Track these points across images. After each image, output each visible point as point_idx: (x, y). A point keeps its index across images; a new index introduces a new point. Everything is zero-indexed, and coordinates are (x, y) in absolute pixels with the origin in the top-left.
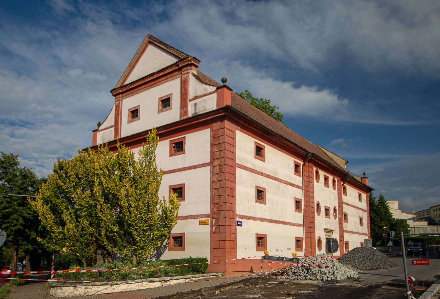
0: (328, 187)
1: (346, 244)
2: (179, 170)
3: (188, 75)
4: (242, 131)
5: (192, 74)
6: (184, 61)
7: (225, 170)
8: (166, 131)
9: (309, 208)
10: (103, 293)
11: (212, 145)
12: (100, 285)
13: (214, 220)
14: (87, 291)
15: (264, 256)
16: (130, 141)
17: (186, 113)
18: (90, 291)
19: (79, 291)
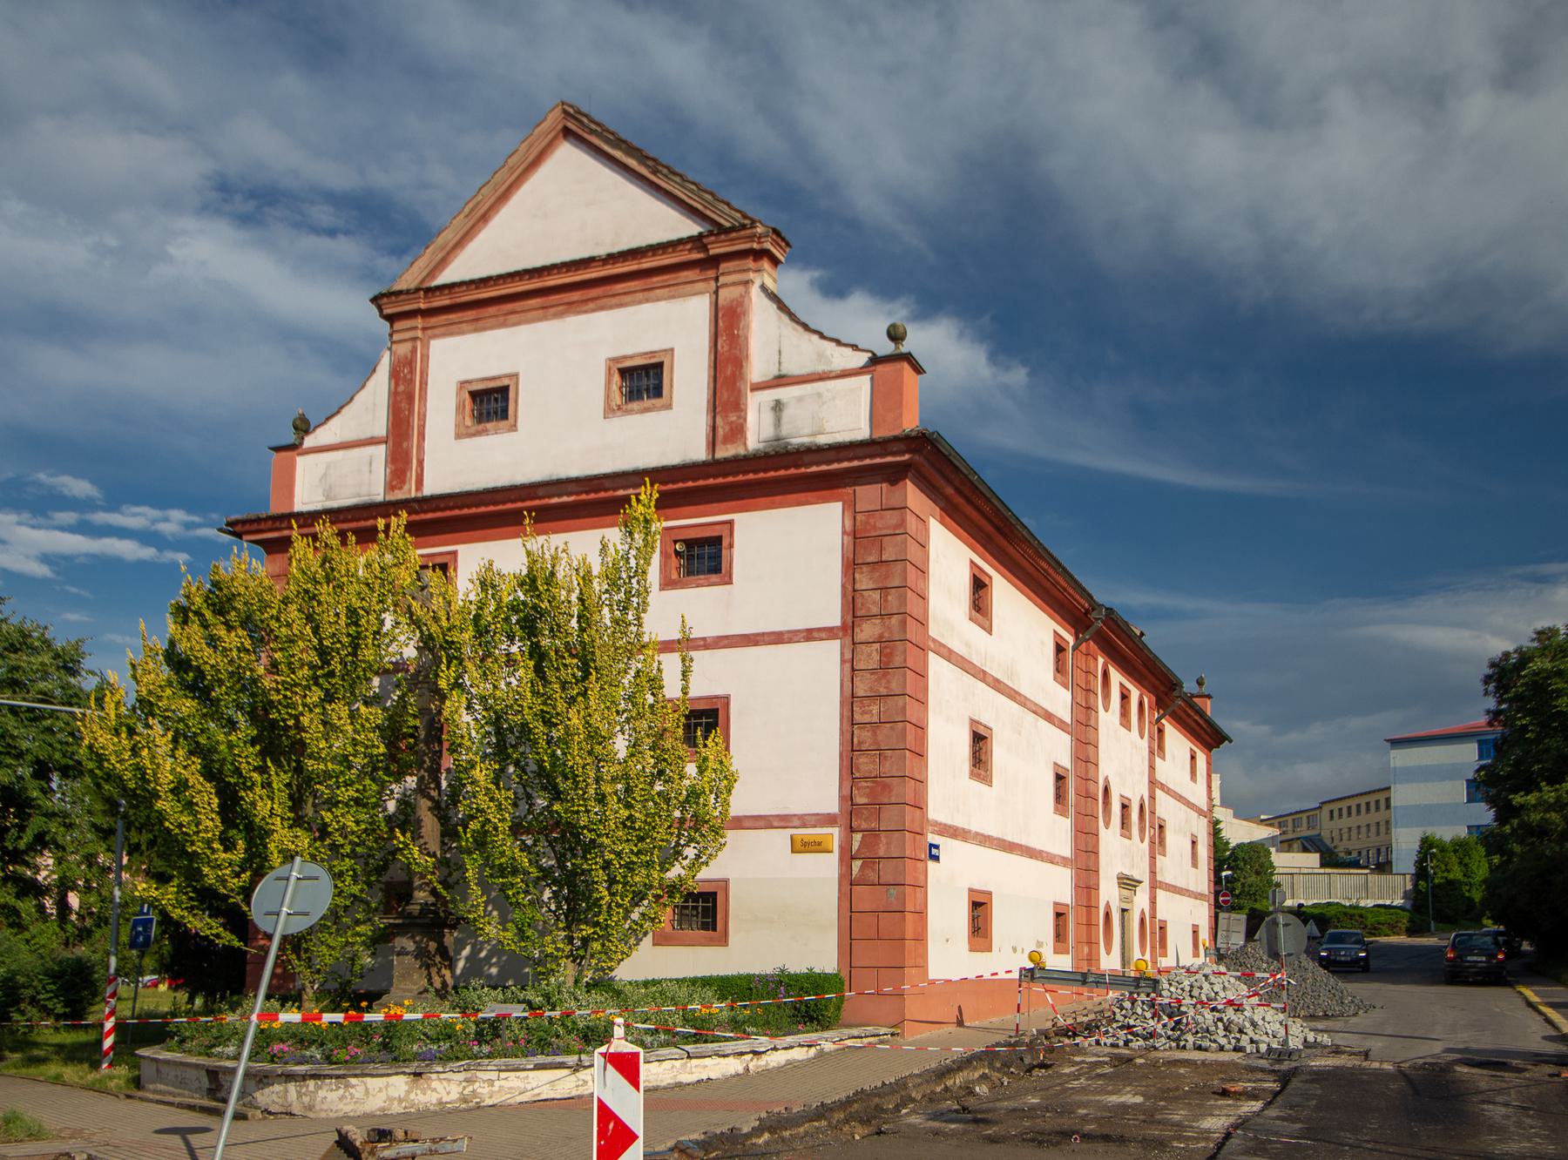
0: (1128, 727)
1: (1161, 928)
2: (702, 643)
3: (747, 291)
4: (942, 522)
5: (763, 288)
6: (734, 235)
7: (905, 661)
9: (1086, 802)
11: (851, 566)
12: (532, 1066)
13: (858, 837)
14: (474, 1091)
15: (1031, 970)
16: (474, 510)
17: (738, 431)
18: (484, 1090)
19: (434, 1090)
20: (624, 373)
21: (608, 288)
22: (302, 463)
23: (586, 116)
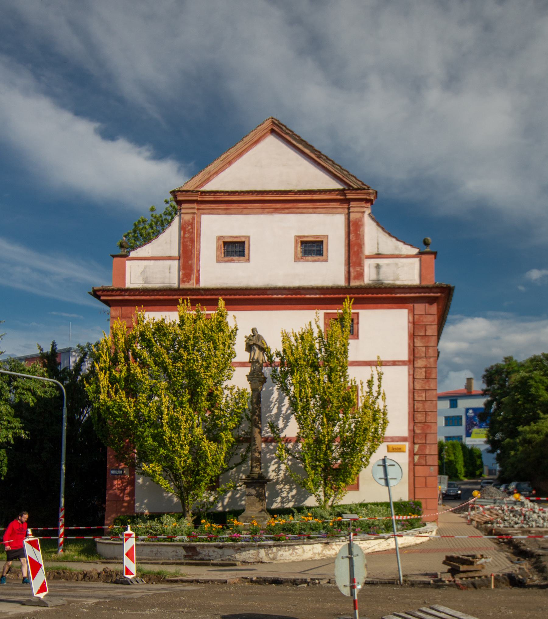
3: (363, 216)
6: (359, 191)
8: (322, 296)
10: (376, 550)
11: (412, 336)
13: (417, 447)
17: (360, 275)
19: (334, 549)
20: (302, 243)
21: (295, 204)
22: (128, 263)
23: (285, 126)
